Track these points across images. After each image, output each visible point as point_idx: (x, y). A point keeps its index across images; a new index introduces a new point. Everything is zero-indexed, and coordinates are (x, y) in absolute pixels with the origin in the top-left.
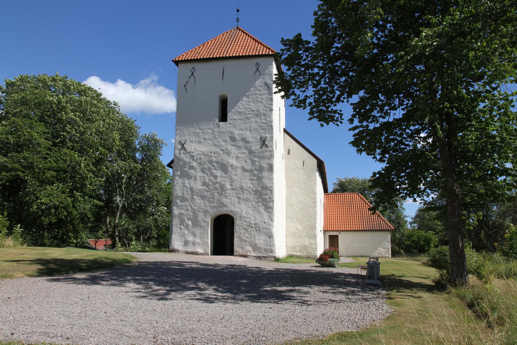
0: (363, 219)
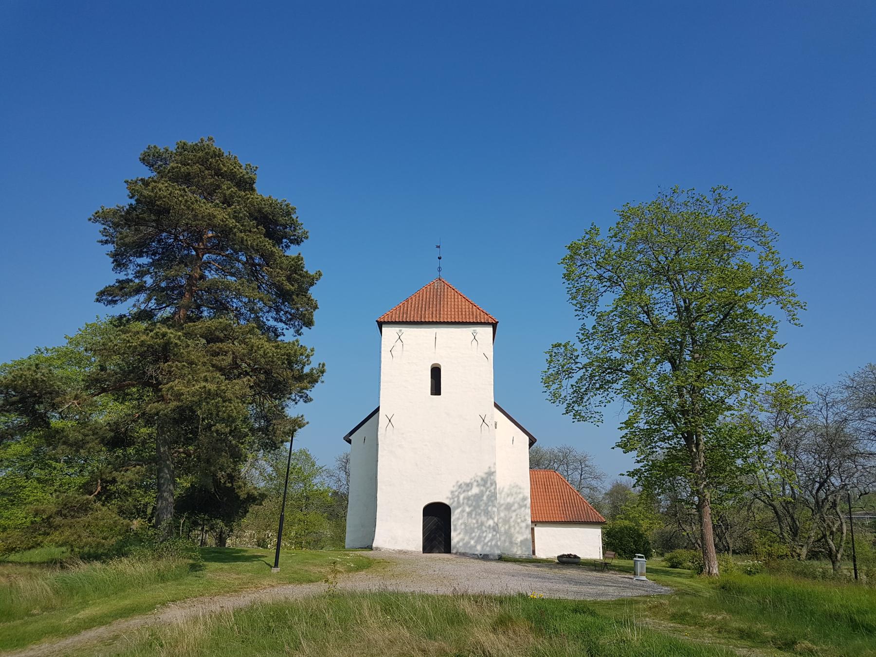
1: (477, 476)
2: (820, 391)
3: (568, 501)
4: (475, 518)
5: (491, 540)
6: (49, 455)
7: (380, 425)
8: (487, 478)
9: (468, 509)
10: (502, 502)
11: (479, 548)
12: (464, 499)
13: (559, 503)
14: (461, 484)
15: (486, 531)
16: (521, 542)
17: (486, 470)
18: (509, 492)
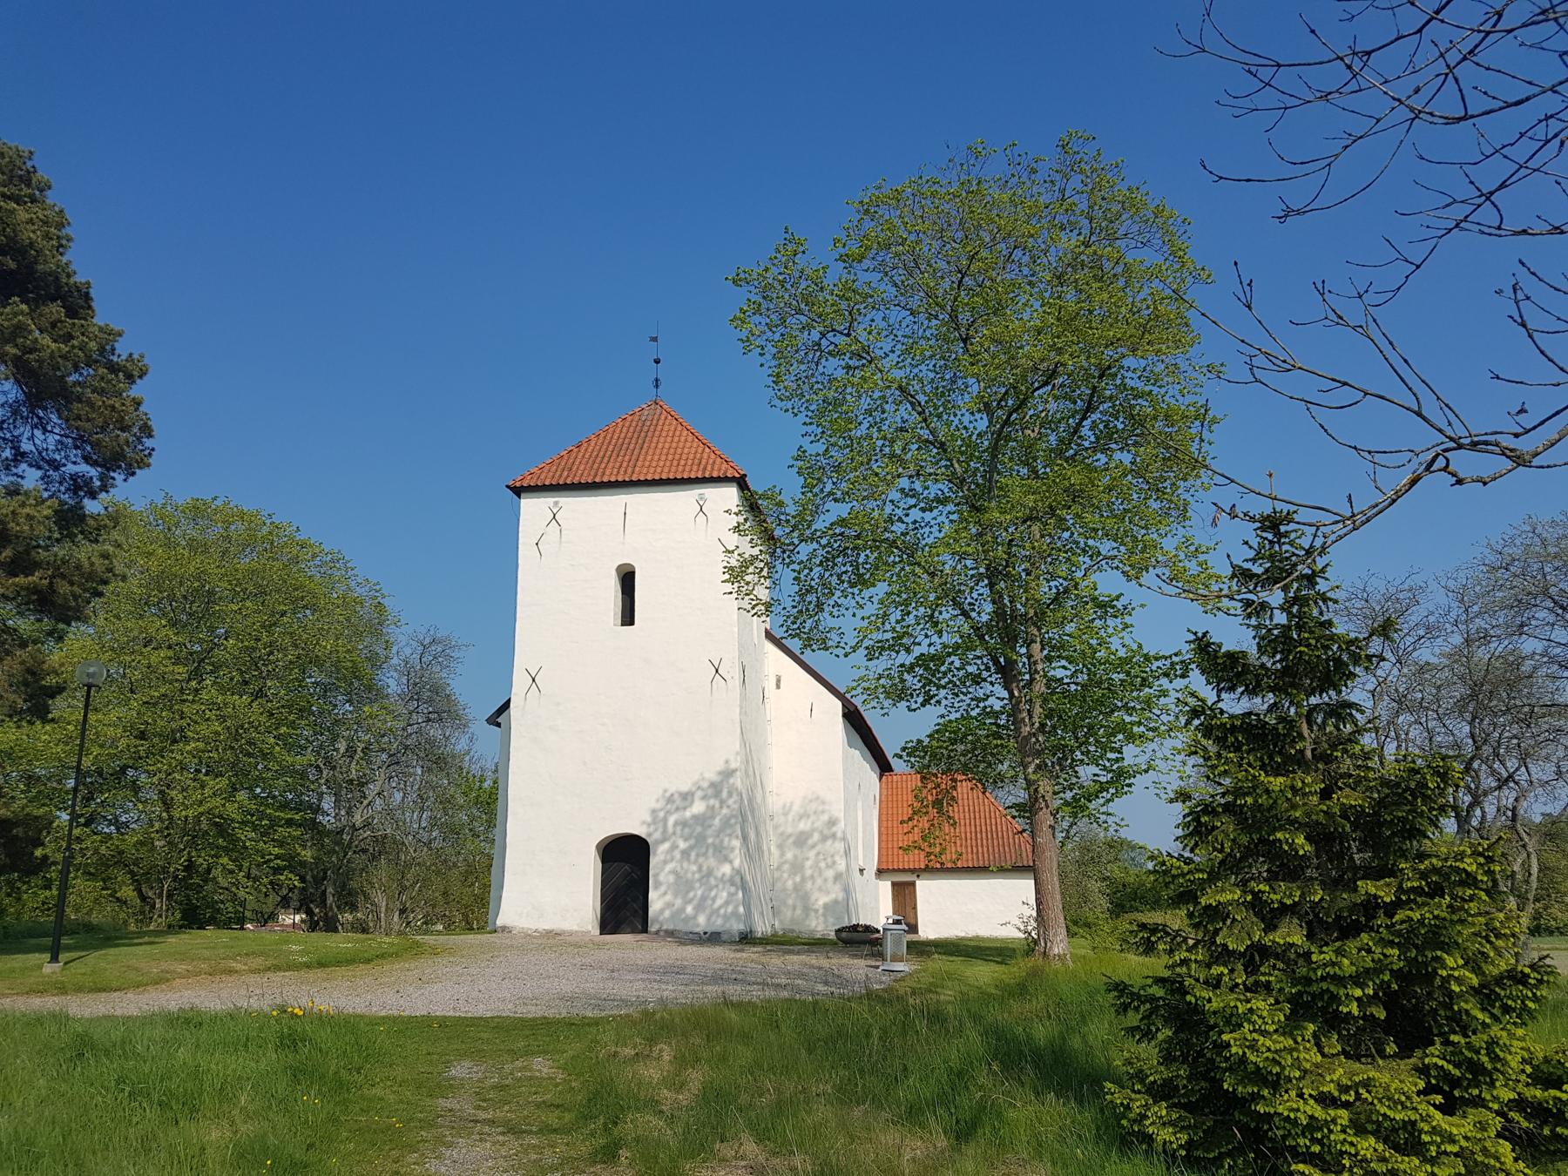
0: (976, 840)
1: (703, 779)
2: (1451, 584)
3: (984, 828)
4: (695, 863)
5: (727, 903)
8: (722, 781)
9: (682, 845)
10: (790, 830)
11: (702, 919)
12: (676, 824)
13: (966, 833)
14: (672, 795)
15: (717, 886)
16: (826, 906)
17: (720, 766)
18: (802, 811)
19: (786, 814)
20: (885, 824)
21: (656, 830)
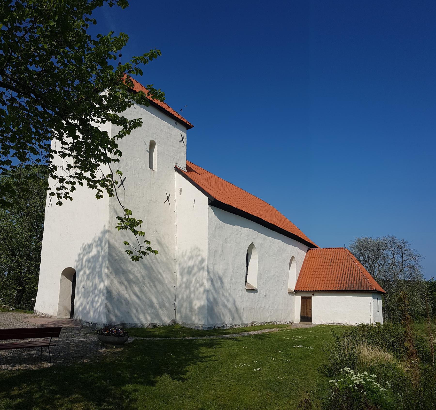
0: (342, 277)
6: (24, 287)
7: (212, 195)
17: (102, 229)
19: (183, 256)
20: (304, 270)
21: (79, 264)
